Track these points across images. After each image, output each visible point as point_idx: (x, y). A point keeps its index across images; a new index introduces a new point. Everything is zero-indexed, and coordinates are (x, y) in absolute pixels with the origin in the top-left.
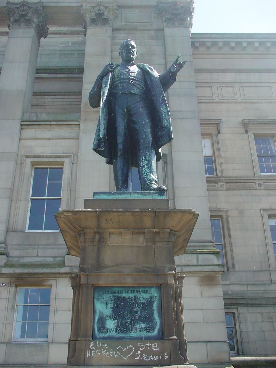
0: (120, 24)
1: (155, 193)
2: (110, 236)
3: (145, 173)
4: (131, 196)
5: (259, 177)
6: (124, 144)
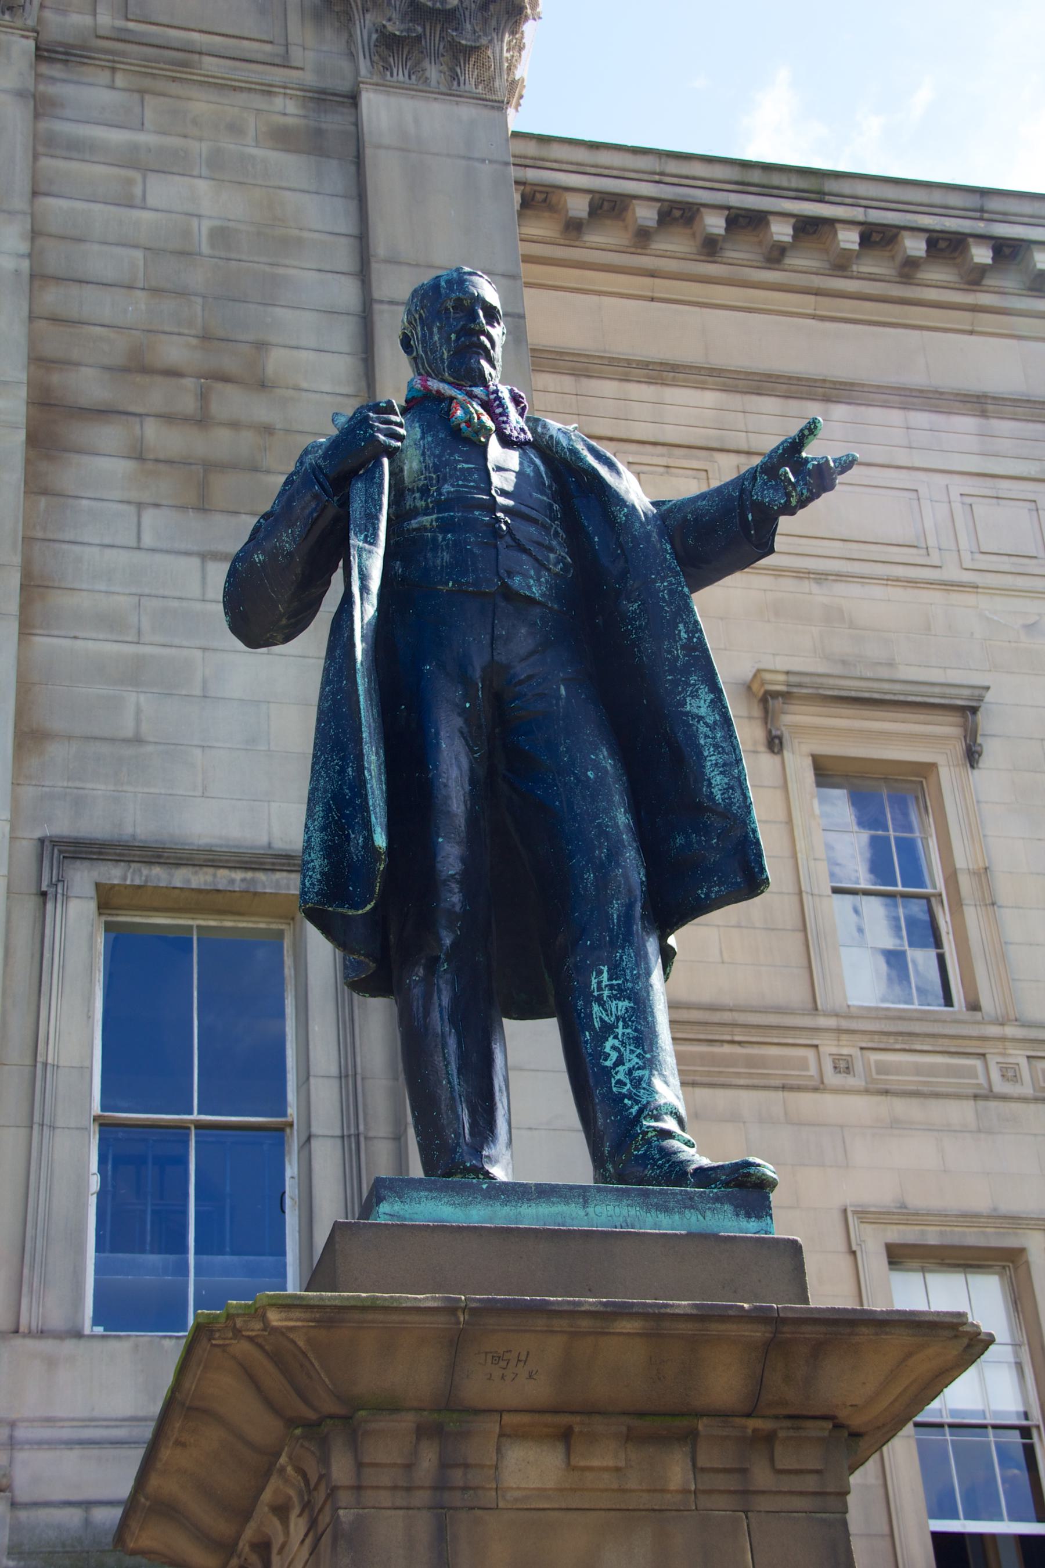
0: (88, 20)
1: (717, 1199)
2: (499, 1450)
3: (620, 1068)
4: (590, 1210)
5: (837, 1015)
6: (468, 879)
